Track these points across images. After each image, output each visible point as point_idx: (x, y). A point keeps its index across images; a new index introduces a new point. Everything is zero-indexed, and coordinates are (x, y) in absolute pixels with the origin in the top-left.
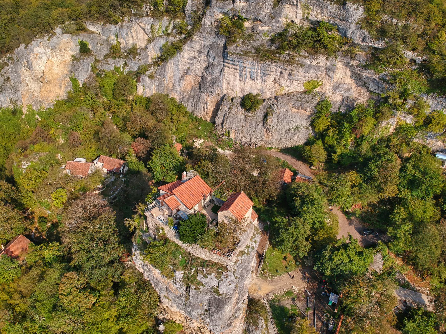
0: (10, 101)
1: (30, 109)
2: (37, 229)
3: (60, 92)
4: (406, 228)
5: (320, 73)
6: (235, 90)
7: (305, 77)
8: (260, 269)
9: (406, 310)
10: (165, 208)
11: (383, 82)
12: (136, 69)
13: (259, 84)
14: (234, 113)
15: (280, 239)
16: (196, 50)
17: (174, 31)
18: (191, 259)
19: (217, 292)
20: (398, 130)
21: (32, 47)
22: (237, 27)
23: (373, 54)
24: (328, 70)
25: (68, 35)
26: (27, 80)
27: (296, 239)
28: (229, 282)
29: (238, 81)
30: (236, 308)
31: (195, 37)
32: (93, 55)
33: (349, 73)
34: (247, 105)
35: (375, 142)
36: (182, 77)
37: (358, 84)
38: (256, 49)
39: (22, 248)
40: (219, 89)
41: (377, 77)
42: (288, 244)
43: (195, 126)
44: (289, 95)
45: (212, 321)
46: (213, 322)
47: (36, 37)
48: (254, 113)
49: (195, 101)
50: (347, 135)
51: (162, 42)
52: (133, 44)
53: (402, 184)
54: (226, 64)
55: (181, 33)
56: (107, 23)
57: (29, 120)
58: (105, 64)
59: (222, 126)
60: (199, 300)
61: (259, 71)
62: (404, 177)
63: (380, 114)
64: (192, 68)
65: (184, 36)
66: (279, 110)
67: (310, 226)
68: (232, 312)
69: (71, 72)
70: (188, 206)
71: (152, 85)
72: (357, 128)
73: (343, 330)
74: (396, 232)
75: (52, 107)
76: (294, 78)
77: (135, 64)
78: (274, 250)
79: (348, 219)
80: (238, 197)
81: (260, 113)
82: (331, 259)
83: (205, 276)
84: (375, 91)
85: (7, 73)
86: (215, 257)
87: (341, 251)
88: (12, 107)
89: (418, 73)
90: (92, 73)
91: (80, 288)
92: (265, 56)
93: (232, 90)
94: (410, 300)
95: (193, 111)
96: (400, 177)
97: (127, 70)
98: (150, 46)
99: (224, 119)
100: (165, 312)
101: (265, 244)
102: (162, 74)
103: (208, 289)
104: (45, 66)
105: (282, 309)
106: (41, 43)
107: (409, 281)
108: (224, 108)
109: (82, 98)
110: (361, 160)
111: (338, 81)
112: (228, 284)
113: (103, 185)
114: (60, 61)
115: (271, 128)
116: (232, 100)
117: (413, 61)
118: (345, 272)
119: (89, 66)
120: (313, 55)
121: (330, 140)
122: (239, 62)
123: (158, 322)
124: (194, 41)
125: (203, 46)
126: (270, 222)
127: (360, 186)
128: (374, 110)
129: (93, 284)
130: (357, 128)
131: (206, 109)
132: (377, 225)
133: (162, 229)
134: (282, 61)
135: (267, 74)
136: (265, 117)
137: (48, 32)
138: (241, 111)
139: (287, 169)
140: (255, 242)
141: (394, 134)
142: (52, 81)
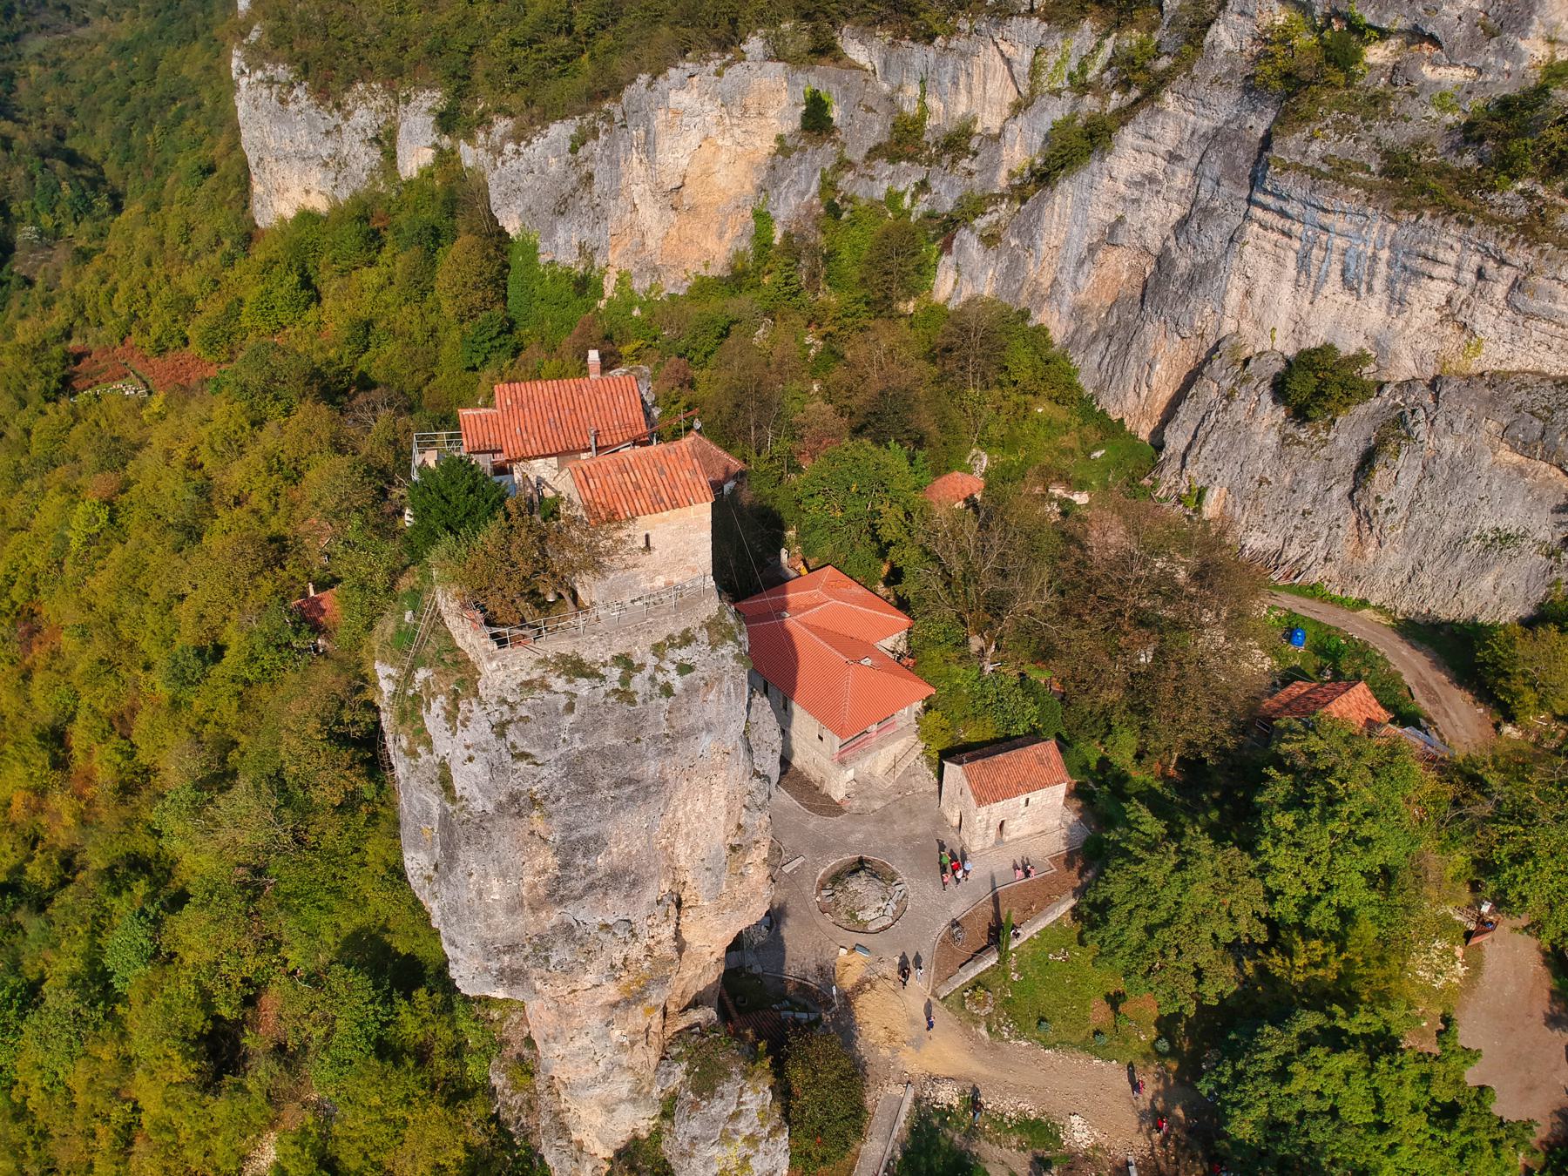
3: (714, 247)
6: (1268, 323)
13: (1374, 312)
16: (1161, 149)
17: (1107, 75)
21: (666, 85)
22: (1328, 60)
25: (781, 64)
29: (1284, 291)
31: (1169, 98)
36: (1092, 250)
38: (1387, 155)
40: (1208, 310)
44: (1496, 381)
48: (1323, 434)
49: (1113, 348)
51: (1056, 111)
54: (1258, 212)
55: (1126, 86)
56: (902, 38)
61: (1385, 255)
64: (1133, 220)
65: (1135, 93)
66: (1440, 440)
68: (526, 924)
71: (984, 268)
76: (1535, 305)
81: (1348, 433)
82: (1282, 1075)
88: (582, 266)
92: (1423, 189)
93: (1258, 322)
95: (1099, 388)
97: (922, 207)
99: (1195, 436)
101: (1047, 901)
102: (1028, 230)
106: (696, 79)
108: (1209, 391)
114: (739, 149)
115: (1381, 512)
124: (1160, 111)
125: (1187, 135)
134: (1492, 221)
135: (1417, 274)
136: (1367, 462)
138: (1271, 416)
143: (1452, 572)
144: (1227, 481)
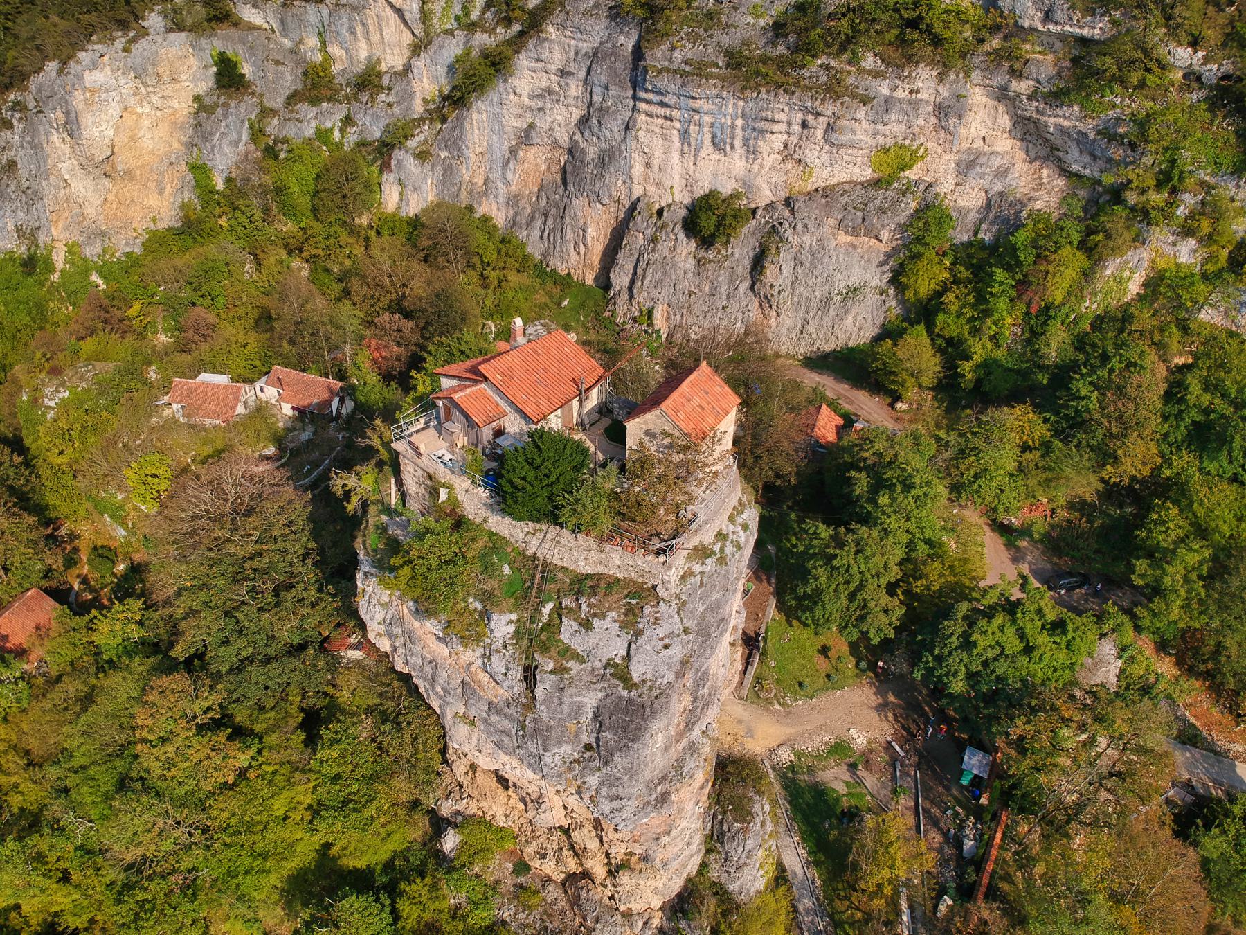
0: (18, 231)
1: (74, 254)
2: (85, 581)
3: (160, 205)
4: (1192, 559)
5: (921, 121)
7: (874, 135)
8: (750, 677)
9: (1194, 804)
10: (457, 427)
11: (1109, 141)
12: (378, 134)
13: (738, 163)
14: (666, 252)
15: (808, 590)
16: (553, 68)
17: (488, 15)
18: (539, 575)
19: (623, 676)
20: (1153, 286)
23: (1075, 61)
24: (942, 111)
25: (183, 34)
26: (64, 167)
27: (860, 587)
28: (662, 639)
30: (684, 742)
31: (550, 29)
32: (253, 93)
33: (1005, 121)
34: (704, 224)
35: (1085, 325)
36: (513, 151)
37: (1033, 155)
38: (729, 54)
39: (38, 628)
41: (1089, 126)
42: (835, 605)
43: (551, 296)
44: (827, 192)
45: (607, 781)
46: (611, 786)
47: (89, 41)
48: (723, 252)
49: (549, 223)
50: (1002, 304)
51: (453, 48)
52: (369, 59)
53: (1171, 439)
55: (507, 21)
57: (73, 287)
58: (289, 120)
59: (631, 296)
60: (566, 708)
61: (739, 122)
62: (1179, 416)
63: (1101, 236)
64: (542, 124)
65: (516, 28)
66: (800, 239)
67: (900, 553)
68: (673, 754)
69: (191, 145)
70: (528, 411)
71: (424, 179)
72: (1031, 283)
73: (1008, 855)
74: (1158, 572)
75: (138, 250)
76: (843, 139)
77: (376, 118)
78: (791, 626)
79: (1010, 545)
80: (691, 377)
81: (741, 250)
82: (967, 644)
83: (586, 625)
84: (1083, 172)
85: (9, 149)
86: (617, 562)
87: (999, 619)
88: (23, 248)
89: (1211, 109)
90: (252, 147)
91: (198, 720)
92: (757, 74)
93: (659, 184)
94: (1202, 778)
95: (546, 254)
96: (1165, 418)
97: (352, 137)
98: (419, 64)
99: (635, 273)
100: (462, 793)
101: (763, 607)
102: (454, 144)
103: (593, 669)
104: (118, 128)
105: (820, 792)
106: (106, 58)
107: (1198, 724)
108: (636, 240)
109: (223, 222)
110: (1043, 379)
111: (974, 146)
112: (661, 644)
113: (281, 449)
114: (159, 113)
115: (776, 294)
116: (660, 213)
117: (1193, 78)
118: (1010, 682)
119: (241, 127)
120: (898, 67)
121: (950, 324)
122: (679, 95)
123: (439, 824)
125: (572, 56)
126: (779, 549)
127: (1046, 447)
128: (1082, 227)
129: (241, 715)
130: (1031, 283)
131: (582, 247)
132: (1100, 557)
133: (448, 486)
135: (763, 132)
136: (758, 264)
137: (124, 26)
138: (686, 247)
139: (824, 406)
140: (745, 527)
141: (1140, 298)
142: (138, 172)
143: (827, 320)
144: (666, 299)
